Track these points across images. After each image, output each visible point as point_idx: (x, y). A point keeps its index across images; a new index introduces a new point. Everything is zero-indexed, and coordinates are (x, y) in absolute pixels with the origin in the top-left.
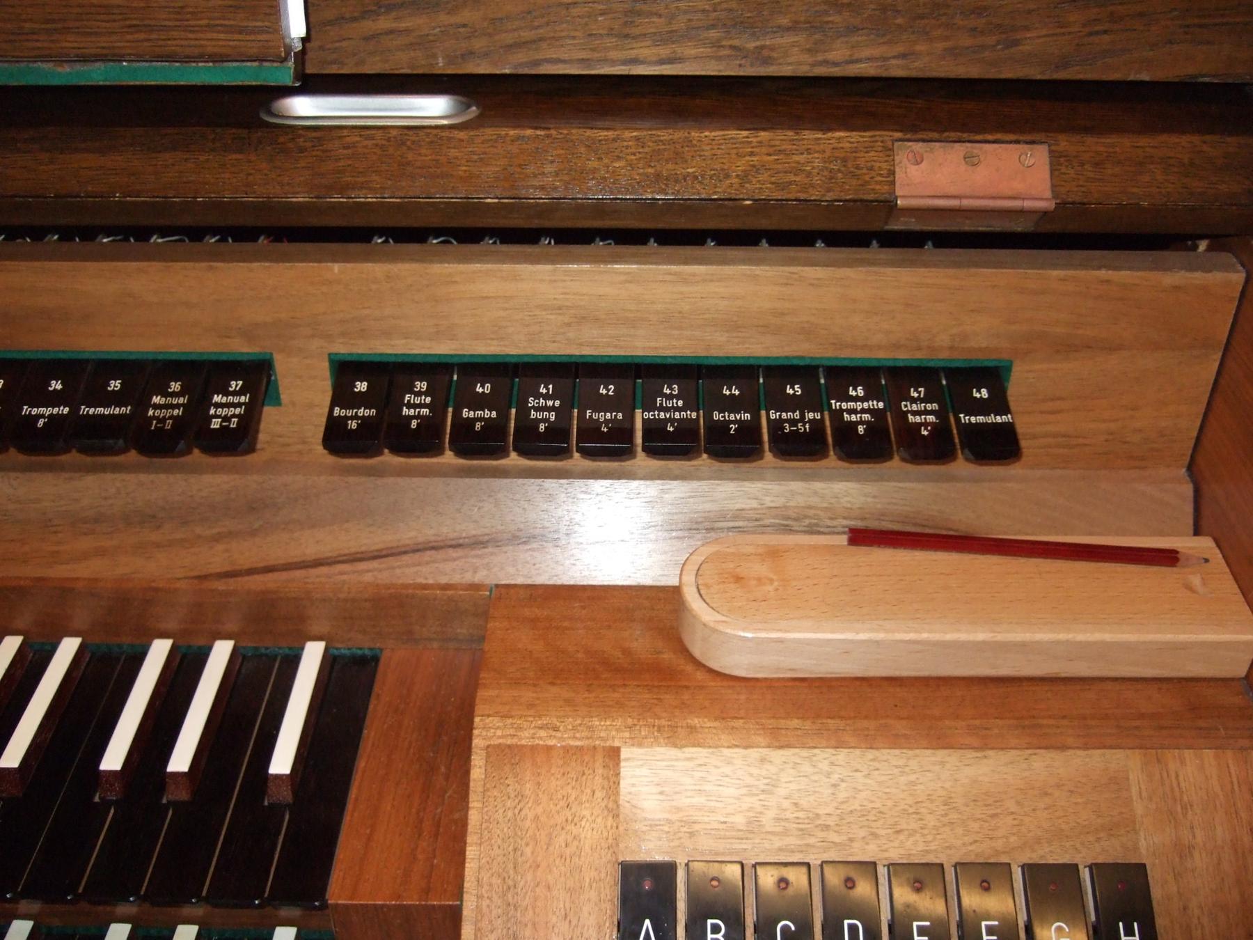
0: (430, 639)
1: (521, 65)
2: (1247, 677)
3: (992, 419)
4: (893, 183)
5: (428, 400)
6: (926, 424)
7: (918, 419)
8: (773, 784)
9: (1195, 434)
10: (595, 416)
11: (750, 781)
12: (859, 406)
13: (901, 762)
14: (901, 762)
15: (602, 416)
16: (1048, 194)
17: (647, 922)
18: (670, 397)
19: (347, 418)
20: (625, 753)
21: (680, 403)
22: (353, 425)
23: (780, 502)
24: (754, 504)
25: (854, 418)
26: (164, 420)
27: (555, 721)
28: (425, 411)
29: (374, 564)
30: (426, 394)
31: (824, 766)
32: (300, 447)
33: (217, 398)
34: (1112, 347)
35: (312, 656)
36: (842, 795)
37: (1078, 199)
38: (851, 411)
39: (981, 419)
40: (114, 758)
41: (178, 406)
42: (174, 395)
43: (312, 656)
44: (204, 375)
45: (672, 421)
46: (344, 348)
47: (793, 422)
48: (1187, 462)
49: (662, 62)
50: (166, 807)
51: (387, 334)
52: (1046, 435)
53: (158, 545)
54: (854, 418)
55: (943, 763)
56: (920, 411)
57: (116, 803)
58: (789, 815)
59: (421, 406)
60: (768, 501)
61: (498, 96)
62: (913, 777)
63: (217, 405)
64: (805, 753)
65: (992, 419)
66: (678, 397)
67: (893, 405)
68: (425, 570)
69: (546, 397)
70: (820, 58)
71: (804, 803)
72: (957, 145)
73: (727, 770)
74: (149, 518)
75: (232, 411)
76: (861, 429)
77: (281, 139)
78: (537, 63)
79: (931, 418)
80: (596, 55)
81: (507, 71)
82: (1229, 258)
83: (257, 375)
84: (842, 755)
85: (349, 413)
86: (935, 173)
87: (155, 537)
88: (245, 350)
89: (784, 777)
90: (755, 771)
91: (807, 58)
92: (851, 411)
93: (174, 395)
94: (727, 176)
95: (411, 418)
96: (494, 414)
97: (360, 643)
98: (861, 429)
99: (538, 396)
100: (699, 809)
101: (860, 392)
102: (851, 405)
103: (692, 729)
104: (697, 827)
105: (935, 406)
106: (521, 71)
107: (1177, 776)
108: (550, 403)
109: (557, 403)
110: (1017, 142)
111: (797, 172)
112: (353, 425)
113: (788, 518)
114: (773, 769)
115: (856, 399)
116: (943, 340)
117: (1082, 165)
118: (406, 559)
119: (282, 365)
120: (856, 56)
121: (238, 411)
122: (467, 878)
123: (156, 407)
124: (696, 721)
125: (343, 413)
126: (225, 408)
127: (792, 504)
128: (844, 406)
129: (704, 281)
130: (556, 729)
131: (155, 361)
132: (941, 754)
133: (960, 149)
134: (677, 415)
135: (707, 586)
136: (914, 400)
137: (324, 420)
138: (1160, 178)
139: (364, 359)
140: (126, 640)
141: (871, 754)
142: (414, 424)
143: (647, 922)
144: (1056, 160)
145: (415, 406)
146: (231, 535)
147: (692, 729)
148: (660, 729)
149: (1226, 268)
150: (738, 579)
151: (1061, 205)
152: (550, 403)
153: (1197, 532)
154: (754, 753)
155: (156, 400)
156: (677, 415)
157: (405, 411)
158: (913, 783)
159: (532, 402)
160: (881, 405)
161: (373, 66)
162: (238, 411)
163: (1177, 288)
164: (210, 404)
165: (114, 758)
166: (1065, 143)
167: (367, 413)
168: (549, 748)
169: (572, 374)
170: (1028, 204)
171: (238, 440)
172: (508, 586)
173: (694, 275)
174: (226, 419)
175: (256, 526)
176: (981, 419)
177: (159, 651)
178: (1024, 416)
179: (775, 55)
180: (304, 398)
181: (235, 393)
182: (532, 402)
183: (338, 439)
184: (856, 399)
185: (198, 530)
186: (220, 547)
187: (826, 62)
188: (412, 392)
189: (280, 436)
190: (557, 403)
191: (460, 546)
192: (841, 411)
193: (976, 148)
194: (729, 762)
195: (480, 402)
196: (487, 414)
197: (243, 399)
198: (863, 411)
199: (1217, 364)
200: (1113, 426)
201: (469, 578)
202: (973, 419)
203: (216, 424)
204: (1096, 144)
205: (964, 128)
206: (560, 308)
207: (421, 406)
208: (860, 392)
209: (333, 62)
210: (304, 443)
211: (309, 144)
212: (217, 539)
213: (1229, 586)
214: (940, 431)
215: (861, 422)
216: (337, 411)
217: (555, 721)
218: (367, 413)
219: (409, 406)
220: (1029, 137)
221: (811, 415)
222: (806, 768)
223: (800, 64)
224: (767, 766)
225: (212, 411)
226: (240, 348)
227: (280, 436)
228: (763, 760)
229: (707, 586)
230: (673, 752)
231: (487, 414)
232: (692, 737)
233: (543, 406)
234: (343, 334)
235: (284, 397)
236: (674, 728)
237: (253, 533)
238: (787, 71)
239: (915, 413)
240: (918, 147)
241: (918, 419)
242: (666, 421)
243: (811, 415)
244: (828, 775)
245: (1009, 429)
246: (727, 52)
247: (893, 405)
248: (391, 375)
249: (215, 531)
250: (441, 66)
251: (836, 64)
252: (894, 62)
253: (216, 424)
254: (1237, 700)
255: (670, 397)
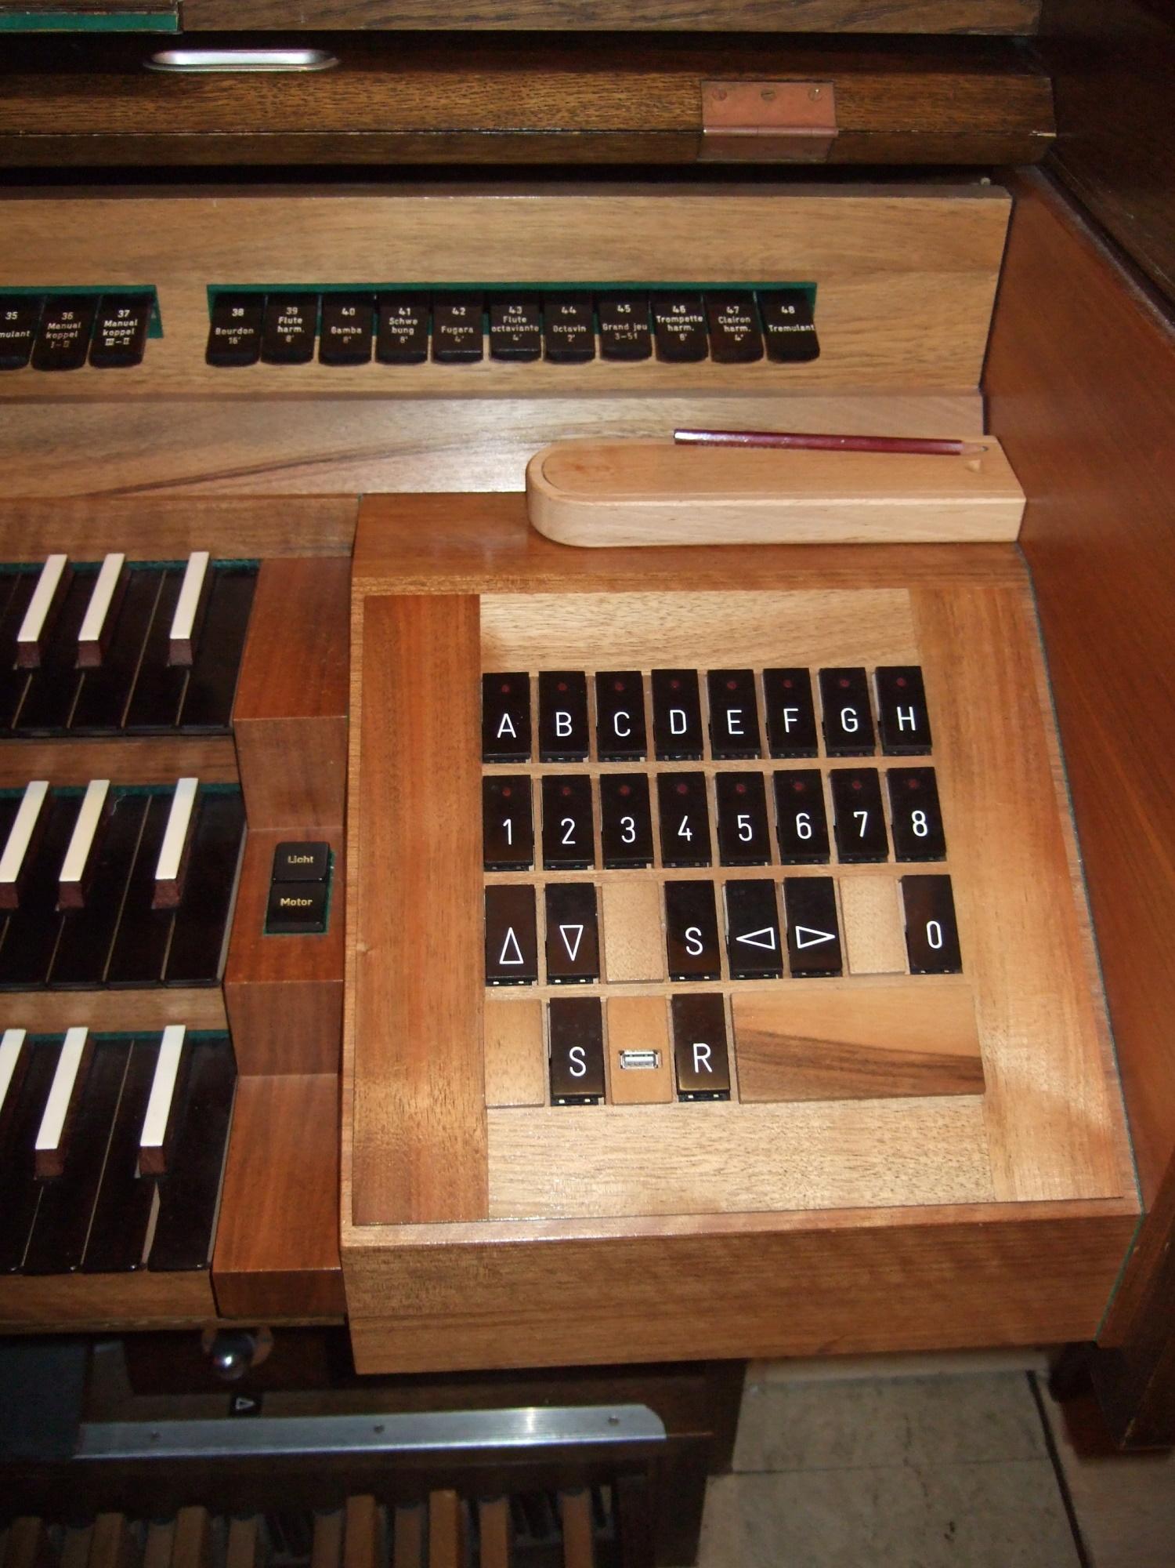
0: (304, 548)
1: (375, 22)
2: (1019, 541)
3: (796, 328)
4: (701, 115)
5: (300, 321)
6: (739, 333)
7: (732, 329)
8: (611, 617)
9: (982, 352)
10: (449, 331)
11: (589, 616)
12: (681, 320)
13: (719, 600)
14: (719, 600)
15: (455, 331)
16: (833, 123)
17: (511, 931)
18: (515, 316)
19: (227, 336)
20: (483, 598)
21: (524, 320)
22: (235, 341)
23: (615, 416)
24: (594, 419)
25: (676, 328)
26: (61, 341)
27: (422, 578)
28: (298, 329)
29: (252, 478)
30: (298, 316)
31: (654, 604)
32: (180, 378)
33: (107, 323)
34: (903, 269)
35: (197, 567)
36: (669, 624)
37: (859, 127)
38: (673, 324)
39: (787, 328)
40: (30, 631)
41: (73, 330)
42: (67, 322)
43: (197, 567)
44: (94, 305)
45: (517, 333)
46: (220, 280)
47: (623, 332)
48: (978, 379)
49: (499, 18)
50: (81, 670)
51: (260, 265)
52: (851, 355)
53: (54, 468)
54: (676, 328)
55: (754, 601)
56: (734, 323)
57: (34, 671)
58: (623, 640)
59: (294, 325)
60: (606, 416)
61: (353, 50)
62: (729, 611)
63: (109, 329)
64: (637, 595)
65: (796, 328)
66: (522, 316)
67: (710, 319)
68: (299, 482)
69: (405, 317)
70: (639, 13)
71: (635, 630)
72: (755, 84)
73: (571, 609)
74: (43, 443)
75: (123, 332)
76: (682, 337)
77: (166, 83)
78: (388, 20)
79: (744, 328)
80: (442, 13)
81: (362, 28)
82: (1003, 190)
83: (142, 303)
84: (669, 596)
85: (230, 332)
86: (740, 110)
87: (50, 460)
88: (132, 283)
89: (619, 613)
90: (596, 609)
91: (626, 13)
92: (673, 324)
93: (67, 322)
94: (559, 111)
95: (285, 334)
96: (359, 330)
97: (239, 552)
98: (682, 337)
99: (398, 316)
100: (545, 636)
101: (683, 309)
102: (674, 319)
103: (541, 582)
104: (545, 651)
105: (748, 319)
106: (375, 27)
107: (951, 607)
108: (409, 322)
109: (415, 322)
110: (807, 81)
111: (618, 107)
112: (235, 341)
113: (624, 430)
114: (610, 607)
115: (679, 315)
116: (754, 264)
117: (862, 99)
118: (282, 473)
119: (163, 296)
120: (671, 12)
121: (129, 332)
122: (352, 695)
123: (52, 331)
124: (544, 576)
125: (224, 332)
126: (116, 329)
127: (628, 417)
128: (668, 320)
129: (543, 210)
130: (423, 584)
131: (49, 295)
132: (753, 594)
133: (758, 87)
134: (522, 329)
135: (552, 473)
136: (730, 316)
137: (205, 341)
138: (929, 109)
139: (240, 290)
140: (23, 558)
141: (694, 594)
142: (289, 339)
143: (511, 931)
144: (841, 96)
145: (288, 326)
146: (120, 456)
147: (541, 582)
148: (513, 582)
149: (1002, 196)
150: (579, 468)
151: (845, 133)
152: (409, 322)
153: (987, 432)
154: (595, 596)
155: (52, 326)
156: (522, 329)
157: (280, 329)
158: (728, 615)
159: (392, 321)
160: (700, 319)
161: (242, 24)
162: (129, 332)
163: (953, 213)
164: (102, 328)
165: (30, 631)
166: (847, 82)
167: (246, 331)
168: (417, 598)
169: (430, 301)
170: (816, 132)
171: (129, 355)
172: (374, 495)
173: (532, 205)
174: (118, 338)
175: (143, 446)
176: (787, 328)
177: (53, 569)
178: (824, 323)
179: (597, 11)
180: (185, 325)
181: (123, 319)
182: (392, 321)
183: (219, 353)
184: (679, 315)
185: (89, 453)
186: (110, 467)
187: (644, 18)
188: (284, 315)
189: (162, 368)
190: (415, 322)
191: (330, 460)
192: (665, 323)
193: (771, 86)
194: (573, 603)
195: (347, 322)
196: (353, 330)
197: (132, 323)
198: (685, 323)
199: (994, 285)
200: (909, 345)
201: (338, 488)
202: (780, 329)
203: (110, 342)
204: (871, 83)
205: (765, 70)
206: (415, 238)
207: (294, 325)
208: (683, 309)
209: (207, 20)
210: (184, 373)
211: (190, 87)
212: (107, 460)
213: (1005, 467)
214: (751, 338)
215: (683, 331)
216: (218, 331)
217: (422, 578)
218: (246, 331)
219: (283, 325)
220: (814, 77)
221: (639, 327)
222: (638, 605)
223: (619, 19)
224: (605, 605)
225: (105, 333)
226: (127, 280)
227: (162, 368)
228: (602, 601)
229: (552, 473)
230: (525, 597)
231: (353, 330)
232: (542, 586)
233: (402, 323)
234: (222, 266)
235: (166, 328)
236: (525, 581)
237: (140, 454)
238: (610, 25)
239: (729, 325)
240: (722, 86)
241: (732, 329)
242: (512, 333)
243: (639, 327)
244: (657, 611)
245: (812, 336)
246: (557, 9)
247: (710, 319)
248: (263, 303)
249: (103, 453)
250: (303, 23)
251: (654, 20)
252: (704, 17)
253: (110, 342)
254: (1011, 557)
255: (515, 316)
